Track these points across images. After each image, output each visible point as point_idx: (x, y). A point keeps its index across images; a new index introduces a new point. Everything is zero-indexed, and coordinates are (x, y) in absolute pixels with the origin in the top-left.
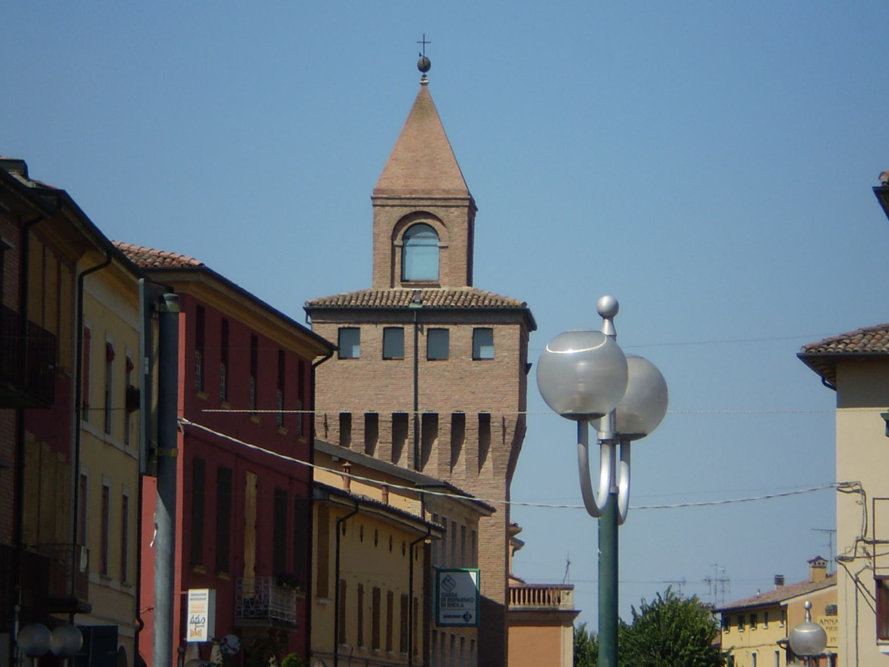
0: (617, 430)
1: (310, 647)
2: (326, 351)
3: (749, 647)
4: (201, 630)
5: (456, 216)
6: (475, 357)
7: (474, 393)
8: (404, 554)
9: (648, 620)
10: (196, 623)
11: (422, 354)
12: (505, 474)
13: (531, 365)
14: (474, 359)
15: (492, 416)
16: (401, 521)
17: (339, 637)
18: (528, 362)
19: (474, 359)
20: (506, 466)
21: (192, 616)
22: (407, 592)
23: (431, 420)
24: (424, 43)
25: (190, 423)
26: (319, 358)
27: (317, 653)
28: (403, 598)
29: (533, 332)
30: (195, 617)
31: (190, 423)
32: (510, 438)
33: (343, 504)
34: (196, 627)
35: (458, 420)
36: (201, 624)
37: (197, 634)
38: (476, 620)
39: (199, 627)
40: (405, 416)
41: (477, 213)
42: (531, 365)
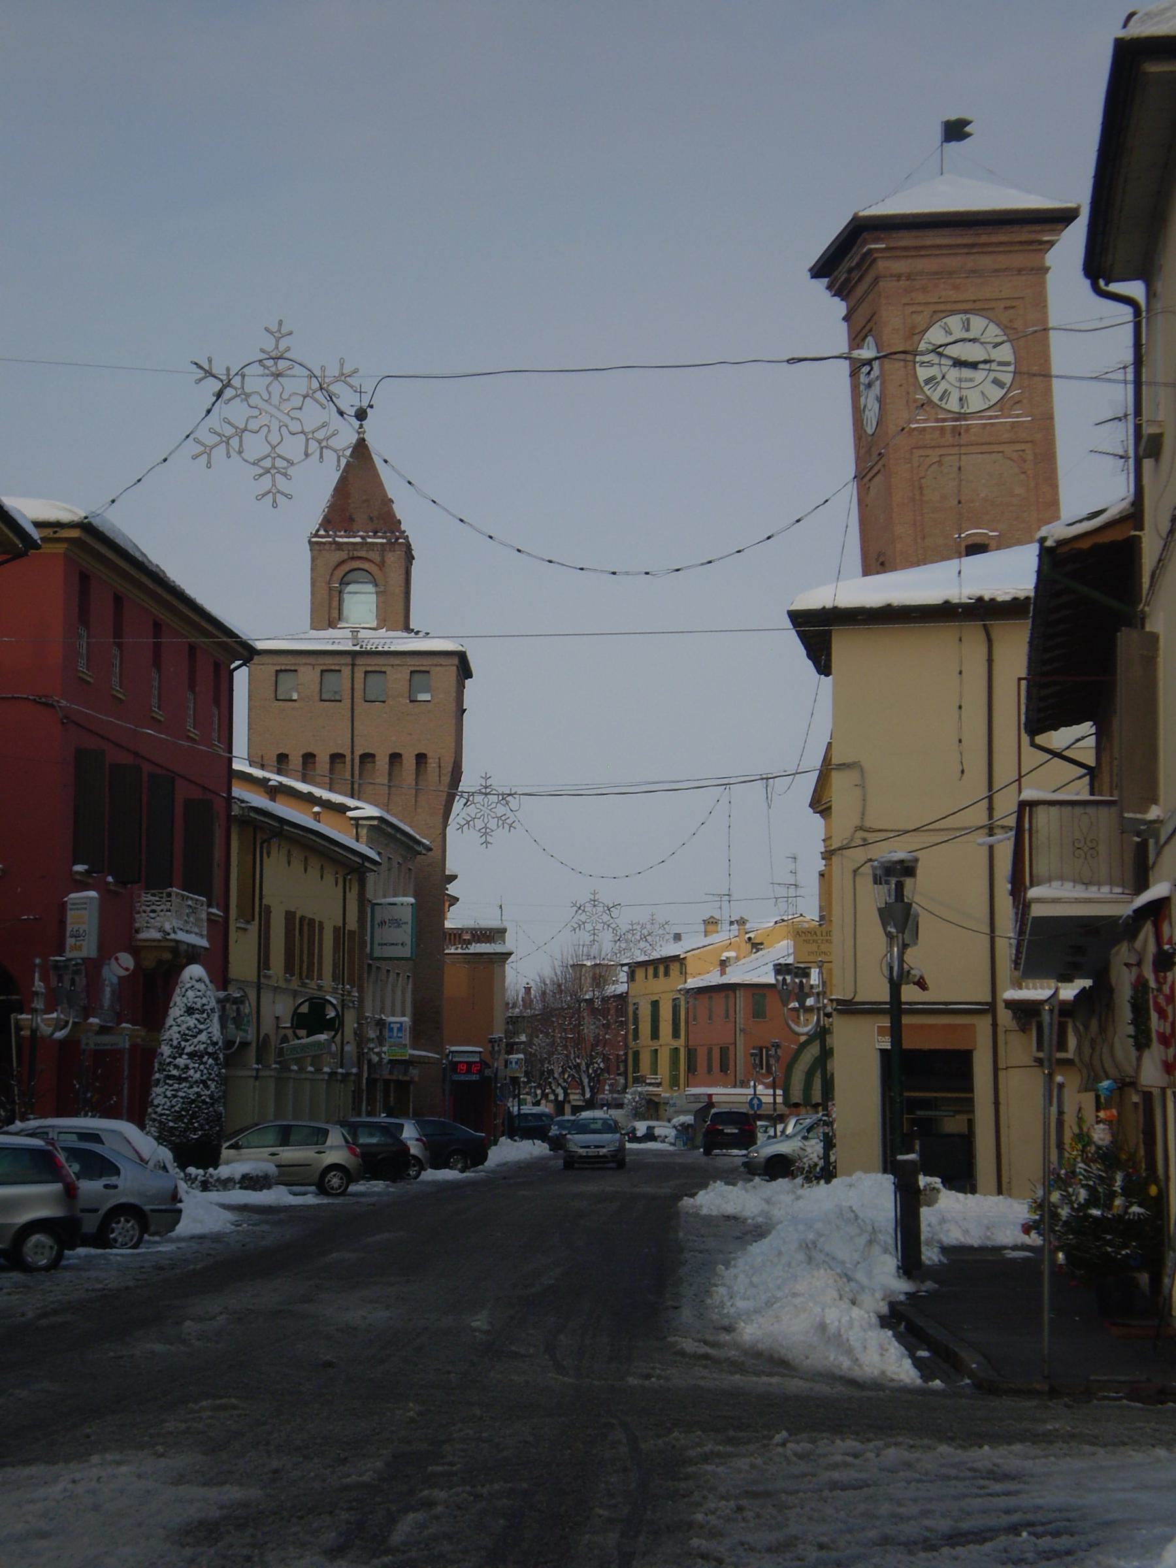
0: (353, 414)
1: (227, 974)
2: (246, 653)
3: (652, 994)
4: (81, 945)
5: (450, 671)
6: (412, 699)
7: (410, 734)
8: (336, 885)
9: (627, 1093)
10: (76, 937)
11: (358, 694)
12: (441, 815)
13: (465, 710)
14: (411, 701)
15: (428, 756)
16: (332, 847)
17: (264, 961)
18: (465, 708)
19: (411, 701)
20: (442, 807)
21: (71, 929)
22: (341, 924)
23: (367, 758)
24: (729, 901)
25: (9, 997)
26: (238, 663)
27: (237, 981)
28: (336, 930)
29: (469, 680)
30: (75, 930)
31: (9, 997)
32: (446, 779)
33: (269, 824)
34: (77, 941)
35: (395, 758)
36: (82, 938)
37: (76, 949)
38: (412, 953)
39: (80, 940)
40: (343, 756)
41: (394, 506)
42: (465, 710)
